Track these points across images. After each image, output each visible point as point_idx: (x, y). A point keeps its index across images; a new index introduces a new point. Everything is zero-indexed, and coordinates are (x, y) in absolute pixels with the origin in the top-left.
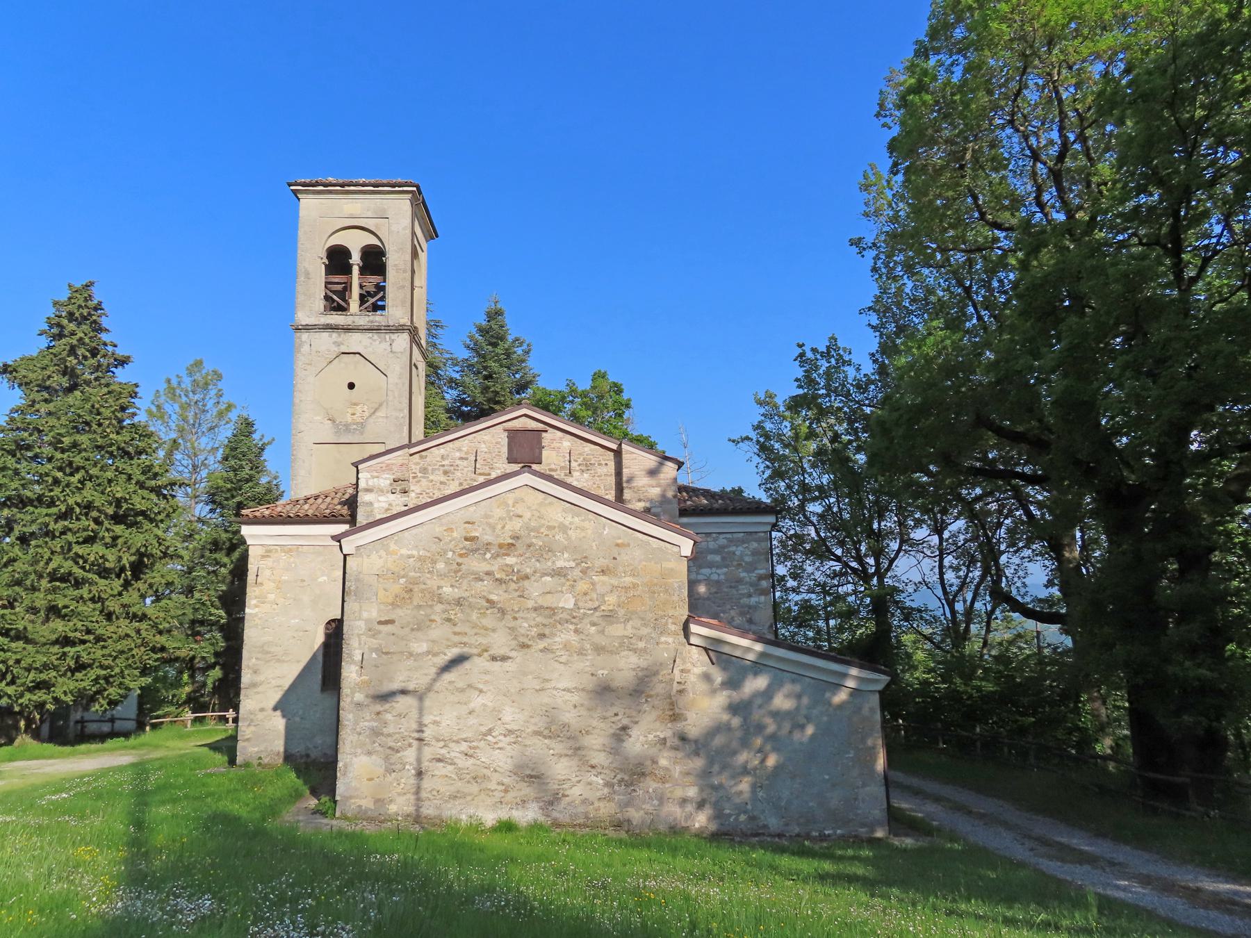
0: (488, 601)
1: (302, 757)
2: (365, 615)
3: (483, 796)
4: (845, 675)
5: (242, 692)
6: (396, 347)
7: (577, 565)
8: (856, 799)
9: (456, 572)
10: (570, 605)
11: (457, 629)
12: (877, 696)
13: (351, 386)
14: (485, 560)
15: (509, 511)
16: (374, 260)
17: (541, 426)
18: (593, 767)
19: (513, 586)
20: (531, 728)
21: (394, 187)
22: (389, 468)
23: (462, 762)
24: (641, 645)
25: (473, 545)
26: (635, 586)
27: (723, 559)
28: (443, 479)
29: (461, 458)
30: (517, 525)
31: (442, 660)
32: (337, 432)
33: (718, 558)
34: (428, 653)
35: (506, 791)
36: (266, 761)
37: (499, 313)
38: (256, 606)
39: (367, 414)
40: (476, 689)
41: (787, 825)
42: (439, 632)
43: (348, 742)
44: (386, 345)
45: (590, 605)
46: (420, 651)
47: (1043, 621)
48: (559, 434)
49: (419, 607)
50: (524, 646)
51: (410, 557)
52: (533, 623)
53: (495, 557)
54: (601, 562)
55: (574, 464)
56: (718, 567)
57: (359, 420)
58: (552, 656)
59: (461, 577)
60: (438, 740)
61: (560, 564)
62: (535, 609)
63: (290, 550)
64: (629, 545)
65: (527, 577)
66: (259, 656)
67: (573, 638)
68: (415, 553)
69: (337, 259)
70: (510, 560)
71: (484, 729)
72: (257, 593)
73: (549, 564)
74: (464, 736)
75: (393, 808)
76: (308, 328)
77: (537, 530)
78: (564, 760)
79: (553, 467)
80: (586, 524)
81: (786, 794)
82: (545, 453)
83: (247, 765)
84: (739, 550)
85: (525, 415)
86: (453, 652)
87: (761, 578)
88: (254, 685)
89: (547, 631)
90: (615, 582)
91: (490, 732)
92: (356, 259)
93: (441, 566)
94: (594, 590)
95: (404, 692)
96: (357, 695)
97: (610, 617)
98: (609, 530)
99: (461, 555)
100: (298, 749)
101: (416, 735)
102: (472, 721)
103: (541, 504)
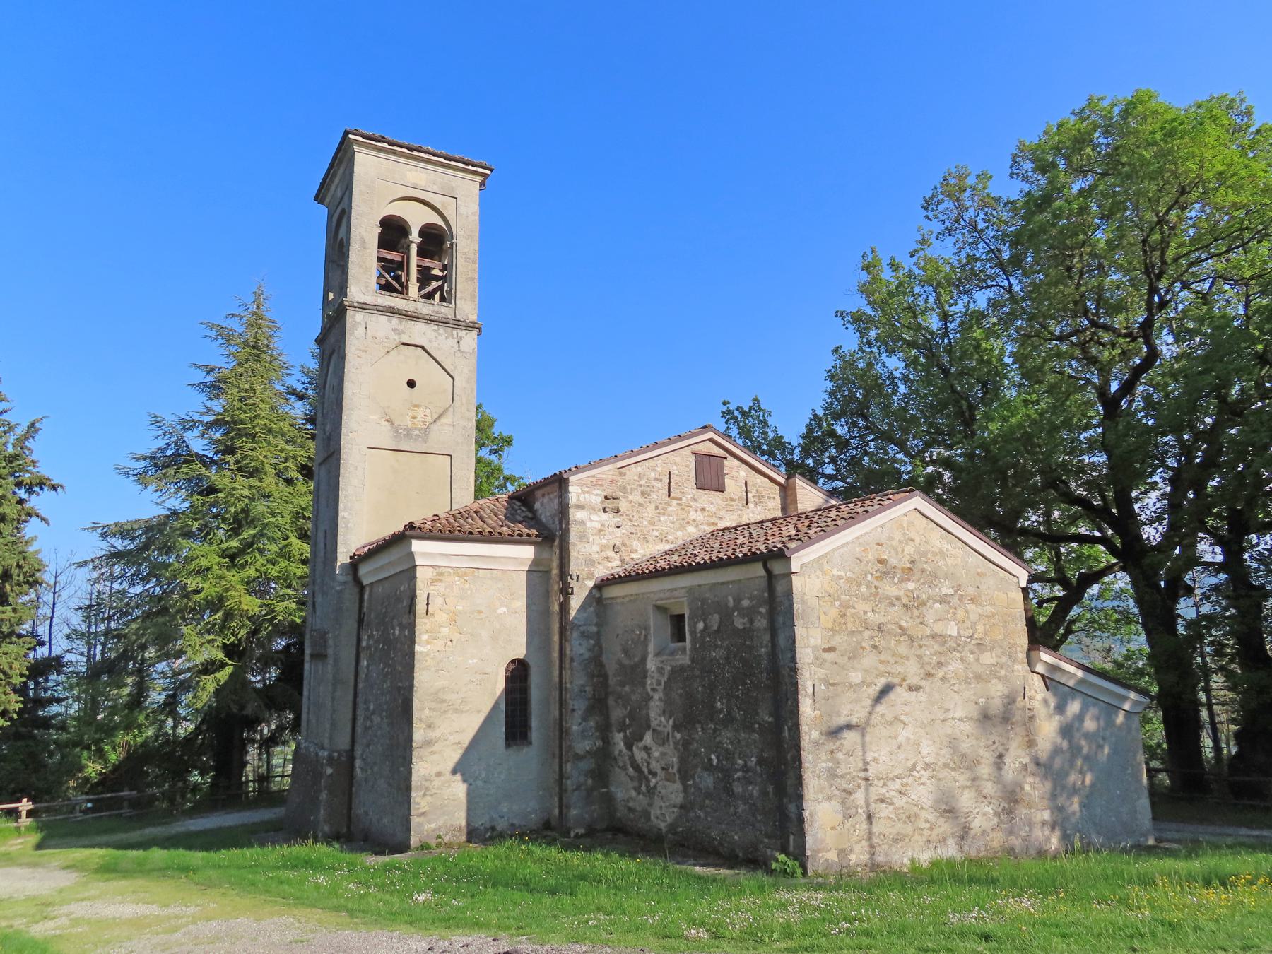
0: (901, 628)
1: (487, 830)
2: (812, 642)
4: (1126, 698)
5: (415, 753)
10: (955, 633)
11: (883, 658)
13: (411, 384)
16: (436, 241)
17: (722, 453)
20: (942, 761)
21: (469, 165)
22: (598, 483)
23: (900, 802)
24: (1003, 672)
25: (885, 570)
26: (993, 615)
28: (641, 500)
29: (656, 479)
30: (910, 549)
31: (873, 691)
32: (397, 437)
35: (931, 829)
36: (447, 839)
38: (428, 643)
39: (429, 419)
42: (869, 660)
43: (810, 787)
48: (736, 462)
50: (929, 675)
51: (840, 578)
53: (902, 580)
57: (421, 425)
60: (879, 779)
63: (465, 574)
66: (433, 705)
68: (843, 574)
69: (393, 232)
70: (911, 585)
71: (910, 764)
72: (428, 626)
75: (853, 858)
78: (966, 792)
82: (727, 481)
83: (424, 847)
85: (711, 440)
86: (881, 682)
88: (428, 743)
91: (914, 765)
92: (415, 237)
95: (849, 727)
100: (481, 822)
101: (862, 774)
102: (901, 756)
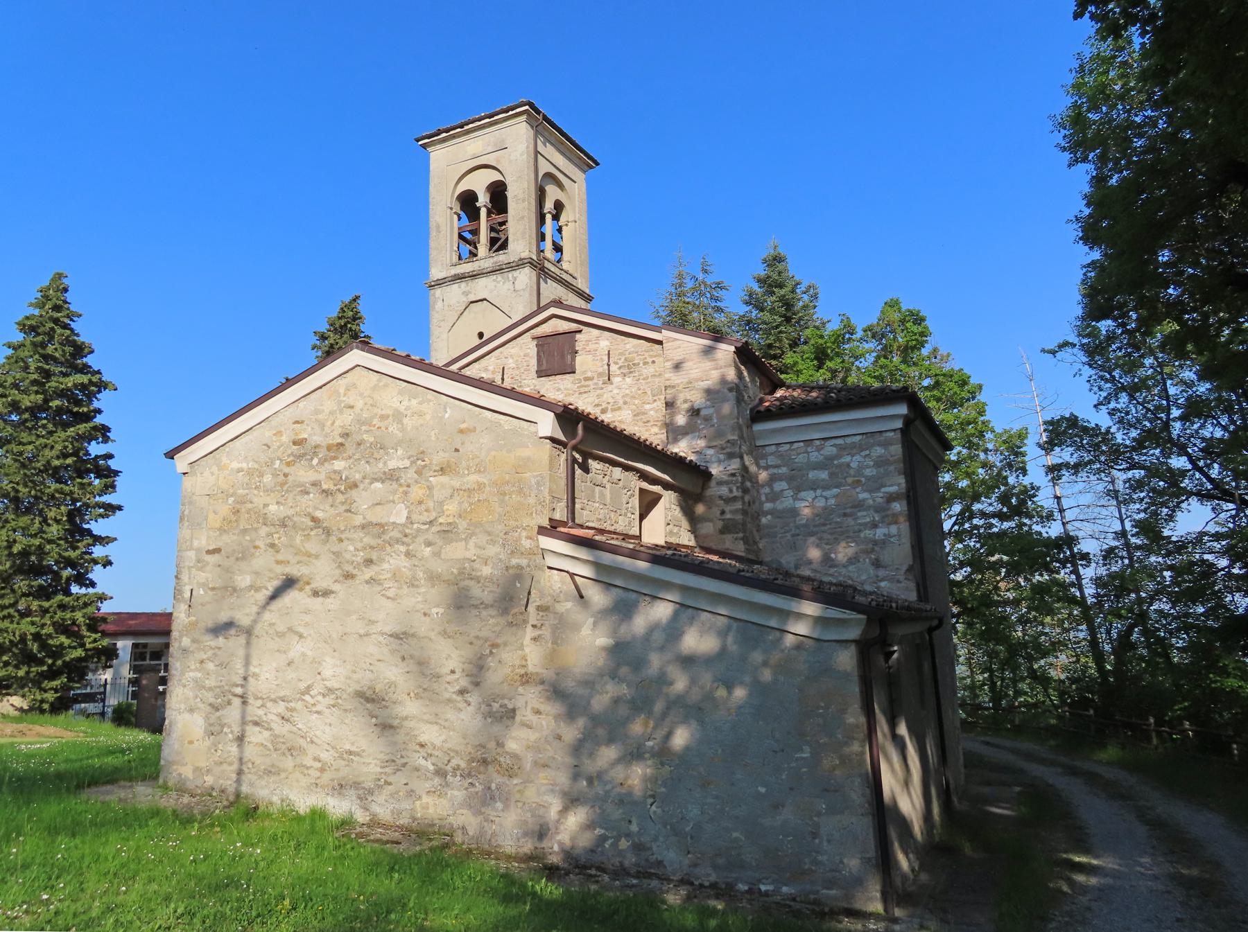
0: (314, 519)
3: (297, 775)
6: (519, 285)
7: (412, 463)
8: (815, 835)
9: (282, 485)
11: (280, 557)
12: (853, 648)
14: (312, 467)
15: (340, 402)
17: (574, 326)
18: (422, 746)
19: (340, 498)
21: (508, 112)
25: (302, 450)
26: (481, 486)
27: (832, 475)
30: (346, 419)
33: (824, 475)
34: (251, 587)
35: (322, 770)
37: (778, 259)
40: (297, 633)
41: (695, 865)
43: (174, 695)
44: (509, 285)
45: (425, 517)
46: (243, 585)
48: (596, 332)
49: (245, 531)
50: (349, 576)
51: (239, 470)
52: (359, 545)
54: (438, 458)
55: (614, 368)
56: (825, 488)
58: (379, 588)
59: (287, 491)
61: (392, 464)
62: (363, 527)
64: (474, 430)
65: (356, 486)
67: (402, 563)
68: (244, 465)
69: (468, 201)
70: (339, 465)
71: (302, 686)
73: (381, 465)
74: (282, 694)
76: (440, 283)
77: (367, 422)
79: (589, 374)
80: (425, 407)
81: (694, 811)
87: (891, 498)
89: (374, 556)
90: (456, 483)
91: (308, 689)
93: (268, 479)
94: (431, 496)
96: (184, 639)
97: (448, 533)
98: (453, 412)
99: (288, 464)
102: (291, 675)
103: (374, 388)
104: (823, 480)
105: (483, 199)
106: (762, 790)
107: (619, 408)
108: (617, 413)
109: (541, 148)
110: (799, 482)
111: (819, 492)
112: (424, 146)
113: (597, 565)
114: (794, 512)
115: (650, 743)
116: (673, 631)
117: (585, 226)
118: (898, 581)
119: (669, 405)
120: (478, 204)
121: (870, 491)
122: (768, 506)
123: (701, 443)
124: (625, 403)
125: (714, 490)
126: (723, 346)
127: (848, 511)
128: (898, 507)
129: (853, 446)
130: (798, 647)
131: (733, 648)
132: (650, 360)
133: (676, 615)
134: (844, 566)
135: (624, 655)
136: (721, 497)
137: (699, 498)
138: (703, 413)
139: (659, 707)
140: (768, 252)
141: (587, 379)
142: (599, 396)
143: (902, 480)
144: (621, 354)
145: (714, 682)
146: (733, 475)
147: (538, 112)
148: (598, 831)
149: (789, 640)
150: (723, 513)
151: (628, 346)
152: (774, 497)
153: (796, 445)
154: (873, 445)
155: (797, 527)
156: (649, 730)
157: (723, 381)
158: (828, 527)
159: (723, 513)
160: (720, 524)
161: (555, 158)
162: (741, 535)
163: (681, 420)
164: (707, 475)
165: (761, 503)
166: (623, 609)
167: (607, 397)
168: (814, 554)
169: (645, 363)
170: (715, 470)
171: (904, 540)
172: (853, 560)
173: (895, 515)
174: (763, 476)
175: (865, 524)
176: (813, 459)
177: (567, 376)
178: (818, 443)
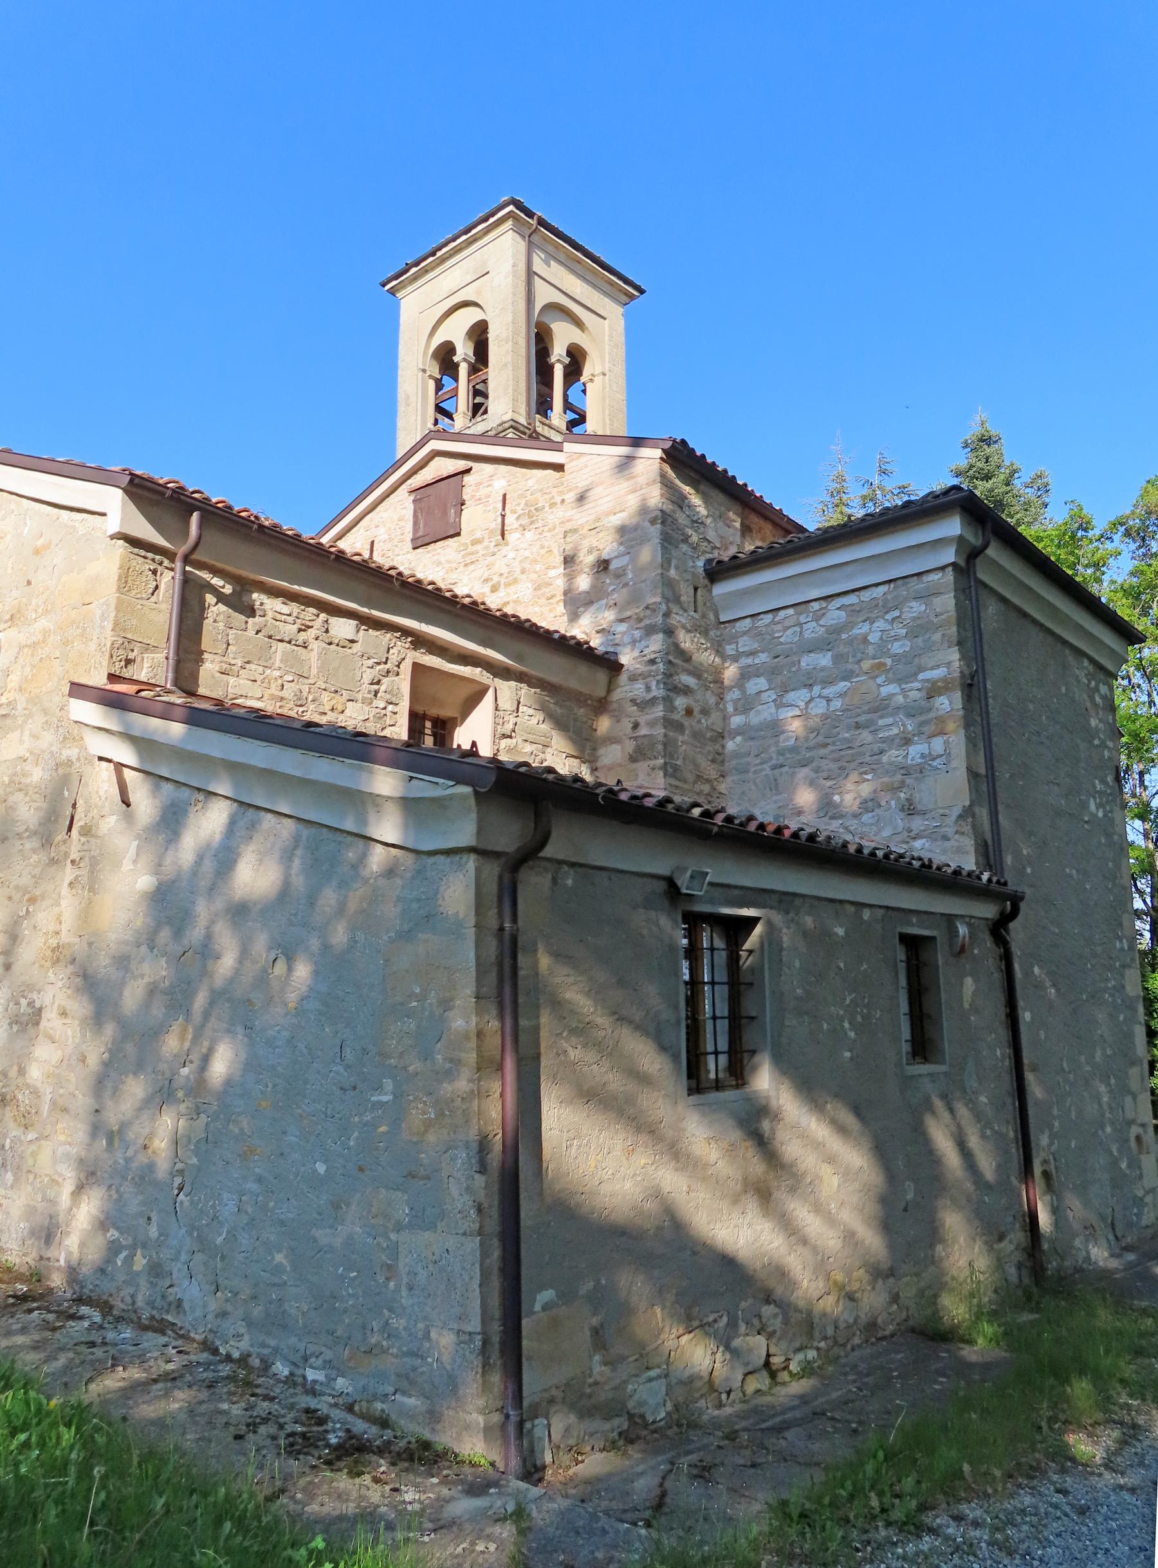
17: (462, 464)
21: (488, 220)
27: (838, 659)
33: (824, 660)
47: (495, 675)
56: (827, 682)
69: (445, 356)
79: (478, 535)
81: (228, 1208)
84: (874, 632)
87: (933, 691)
104: (823, 669)
105: (464, 351)
106: (321, 1168)
107: (516, 581)
108: (512, 589)
109: (538, 265)
110: (785, 676)
111: (817, 690)
112: (393, 292)
113: (142, 743)
114: (775, 728)
115: (185, 1071)
116: (224, 859)
117: (622, 382)
118: (945, 838)
119: (569, 560)
120: (456, 359)
121: (900, 681)
122: (736, 721)
123: (610, 616)
124: (523, 572)
125: (626, 690)
126: (645, 452)
127: (862, 719)
128: (949, 704)
129: (874, 604)
130: (390, 872)
131: (299, 881)
132: (558, 499)
133: (232, 823)
134: (856, 816)
135: (168, 904)
136: (633, 701)
137: (601, 706)
138: (613, 566)
139: (200, 1000)
140: (973, 431)
141: (475, 542)
142: (489, 566)
143: (954, 655)
144: (521, 496)
145: (270, 948)
146: (652, 662)
147: (530, 214)
148: (113, 1234)
149: (378, 857)
150: (636, 726)
151: (530, 483)
152: (746, 705)
153: (782, 613)
154: (906, 599)
155: (781, 753)
156: (187, 1044)
157: (643, 510)
158: (829, 750)
159: (636, 726)
160: (630, 746)
161: (561, 281)
162: (661, 761)
163: (584, 583)
164: (610, 665)
165: (725, 718)
166: (171, 822)
167: (500, 565)
168: (806, 797)
169: (553, 505)
170: (624, 660)
171: (954, 764)
172: (869, 805)
173: (941, 720)
174: (730, 672)
175: (891, 739)
176: (807, 635)
177: (450, 542)
178: (816, 606)
